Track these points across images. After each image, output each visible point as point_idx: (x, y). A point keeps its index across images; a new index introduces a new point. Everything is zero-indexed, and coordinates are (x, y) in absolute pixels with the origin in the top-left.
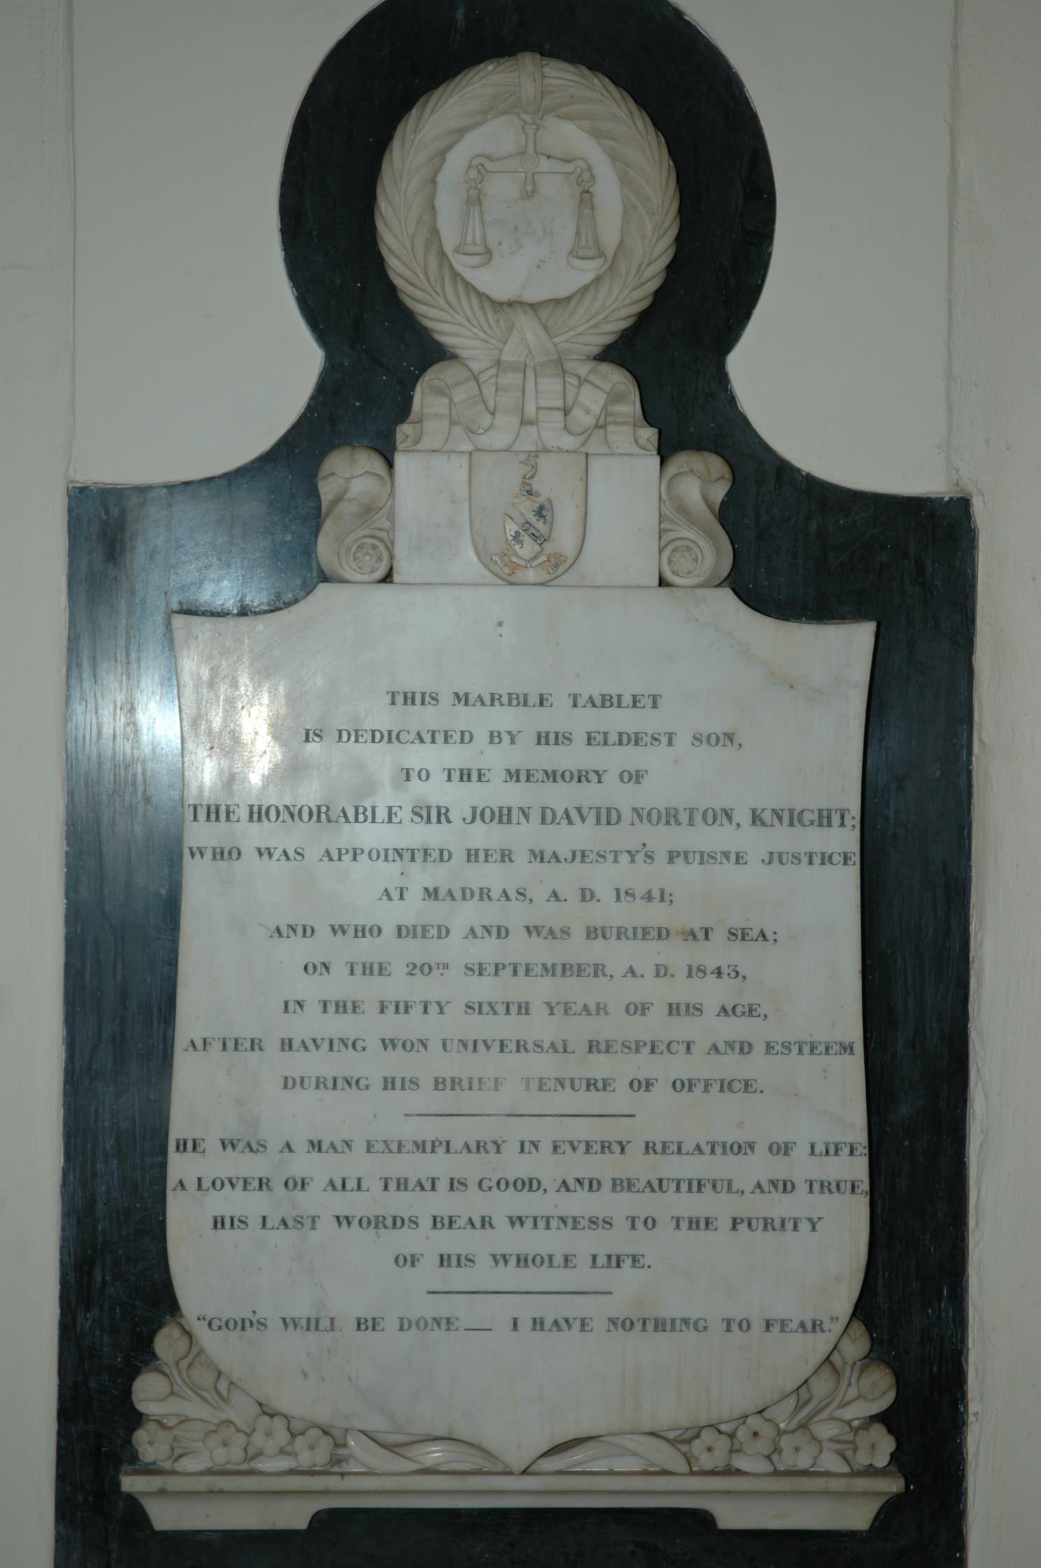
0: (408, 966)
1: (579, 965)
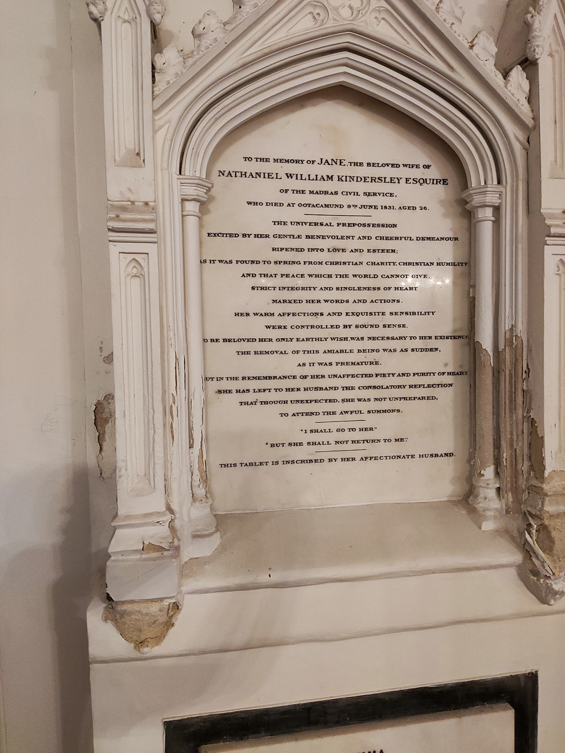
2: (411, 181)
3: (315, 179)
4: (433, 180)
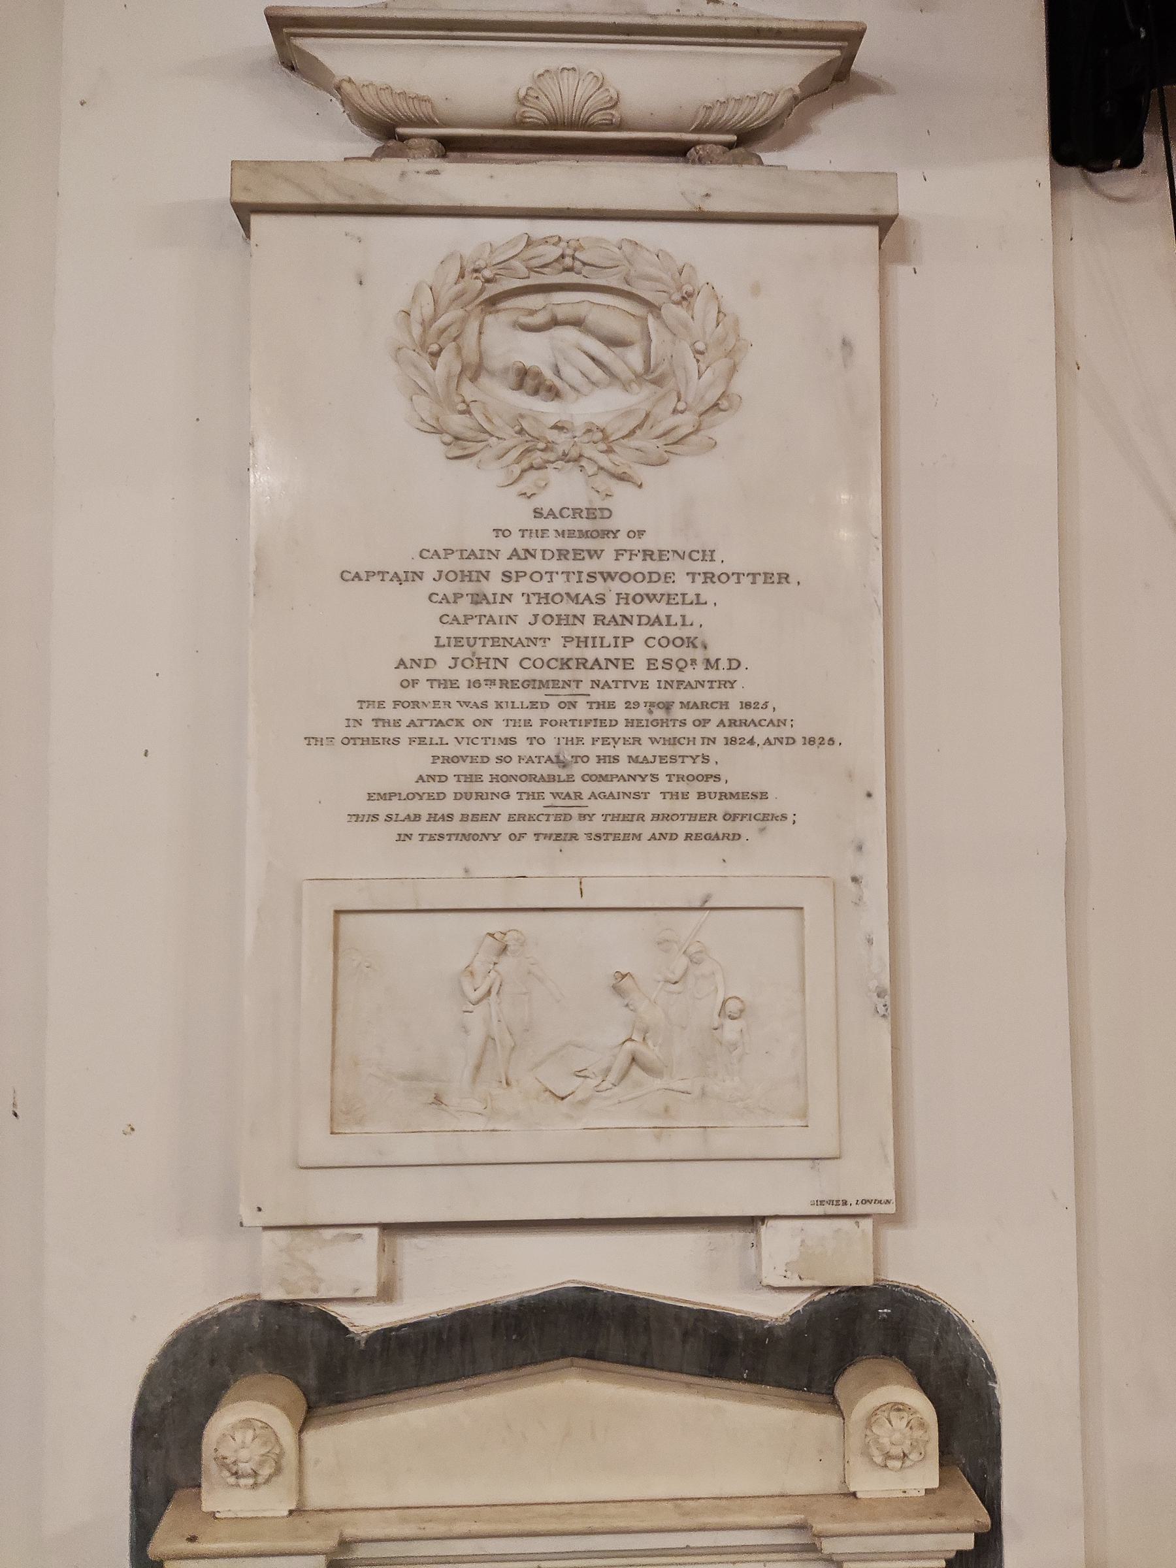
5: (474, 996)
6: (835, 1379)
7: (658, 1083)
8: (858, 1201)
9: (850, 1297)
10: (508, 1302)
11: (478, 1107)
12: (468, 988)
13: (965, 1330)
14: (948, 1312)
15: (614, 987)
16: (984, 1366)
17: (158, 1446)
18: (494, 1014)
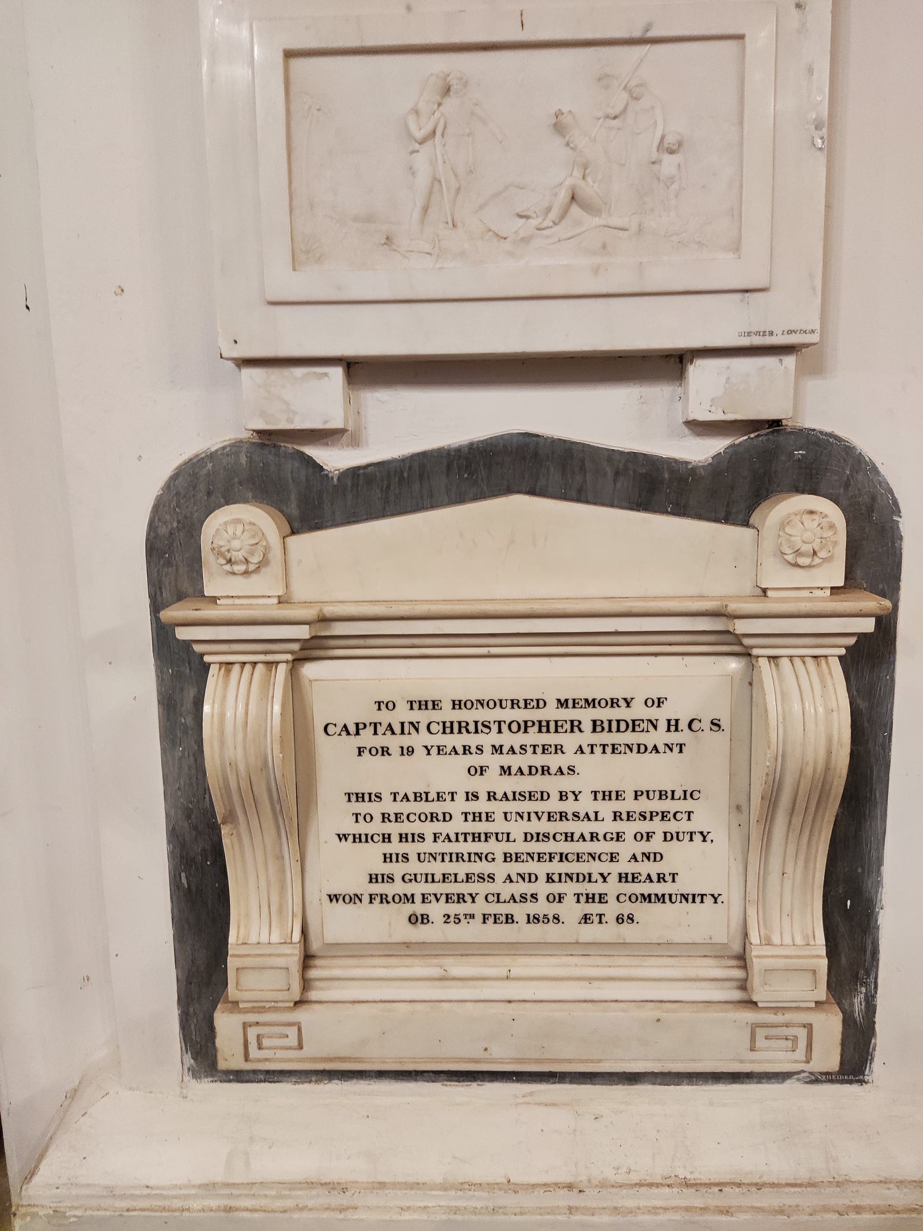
0: (444, 916)
1: (516, 854)
2: (585, 857)
3: (682, 797)
4: (427, 875)
5: (419, 135)
6: (751, 513)
7: (597, 221)
8: (784, 331)
9: (768, 439)
10: (459, 446)
11: (427, 247)
12: (413, 127)
13: (875, 469)
14: (860, 453)
15: (555, 125)
16: (890, 502)
17: (169, 564)
18: (439, 156)
